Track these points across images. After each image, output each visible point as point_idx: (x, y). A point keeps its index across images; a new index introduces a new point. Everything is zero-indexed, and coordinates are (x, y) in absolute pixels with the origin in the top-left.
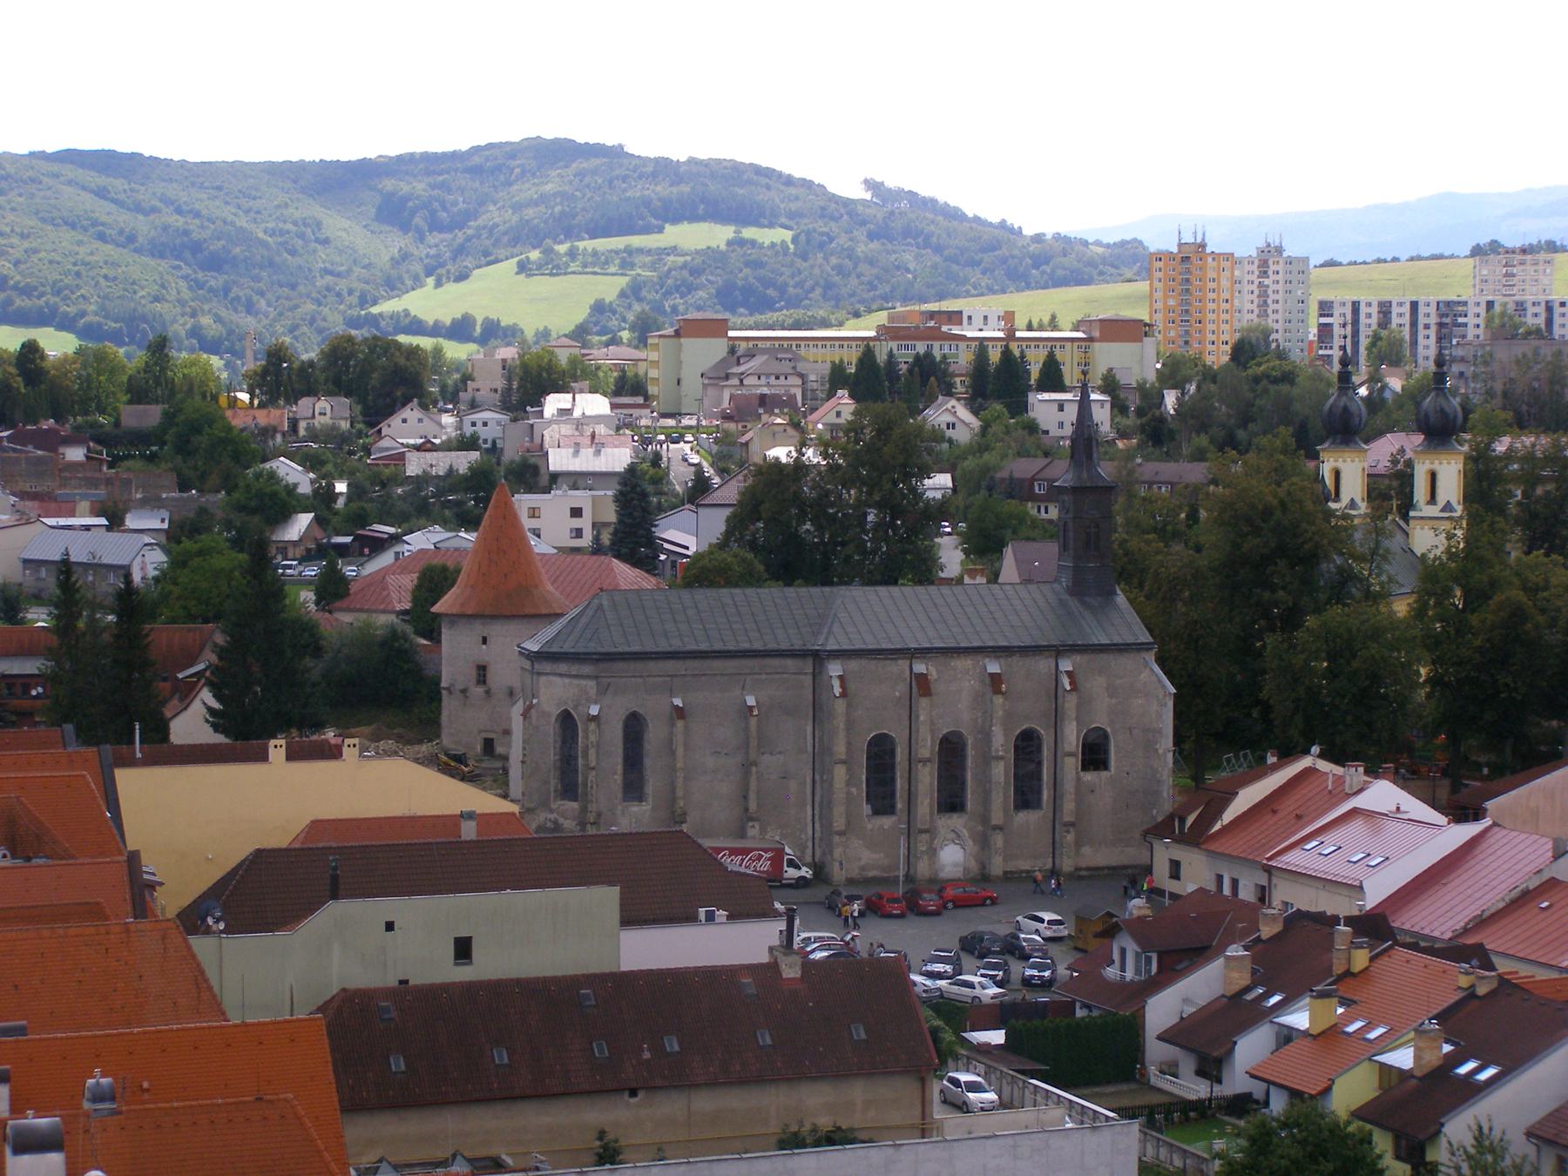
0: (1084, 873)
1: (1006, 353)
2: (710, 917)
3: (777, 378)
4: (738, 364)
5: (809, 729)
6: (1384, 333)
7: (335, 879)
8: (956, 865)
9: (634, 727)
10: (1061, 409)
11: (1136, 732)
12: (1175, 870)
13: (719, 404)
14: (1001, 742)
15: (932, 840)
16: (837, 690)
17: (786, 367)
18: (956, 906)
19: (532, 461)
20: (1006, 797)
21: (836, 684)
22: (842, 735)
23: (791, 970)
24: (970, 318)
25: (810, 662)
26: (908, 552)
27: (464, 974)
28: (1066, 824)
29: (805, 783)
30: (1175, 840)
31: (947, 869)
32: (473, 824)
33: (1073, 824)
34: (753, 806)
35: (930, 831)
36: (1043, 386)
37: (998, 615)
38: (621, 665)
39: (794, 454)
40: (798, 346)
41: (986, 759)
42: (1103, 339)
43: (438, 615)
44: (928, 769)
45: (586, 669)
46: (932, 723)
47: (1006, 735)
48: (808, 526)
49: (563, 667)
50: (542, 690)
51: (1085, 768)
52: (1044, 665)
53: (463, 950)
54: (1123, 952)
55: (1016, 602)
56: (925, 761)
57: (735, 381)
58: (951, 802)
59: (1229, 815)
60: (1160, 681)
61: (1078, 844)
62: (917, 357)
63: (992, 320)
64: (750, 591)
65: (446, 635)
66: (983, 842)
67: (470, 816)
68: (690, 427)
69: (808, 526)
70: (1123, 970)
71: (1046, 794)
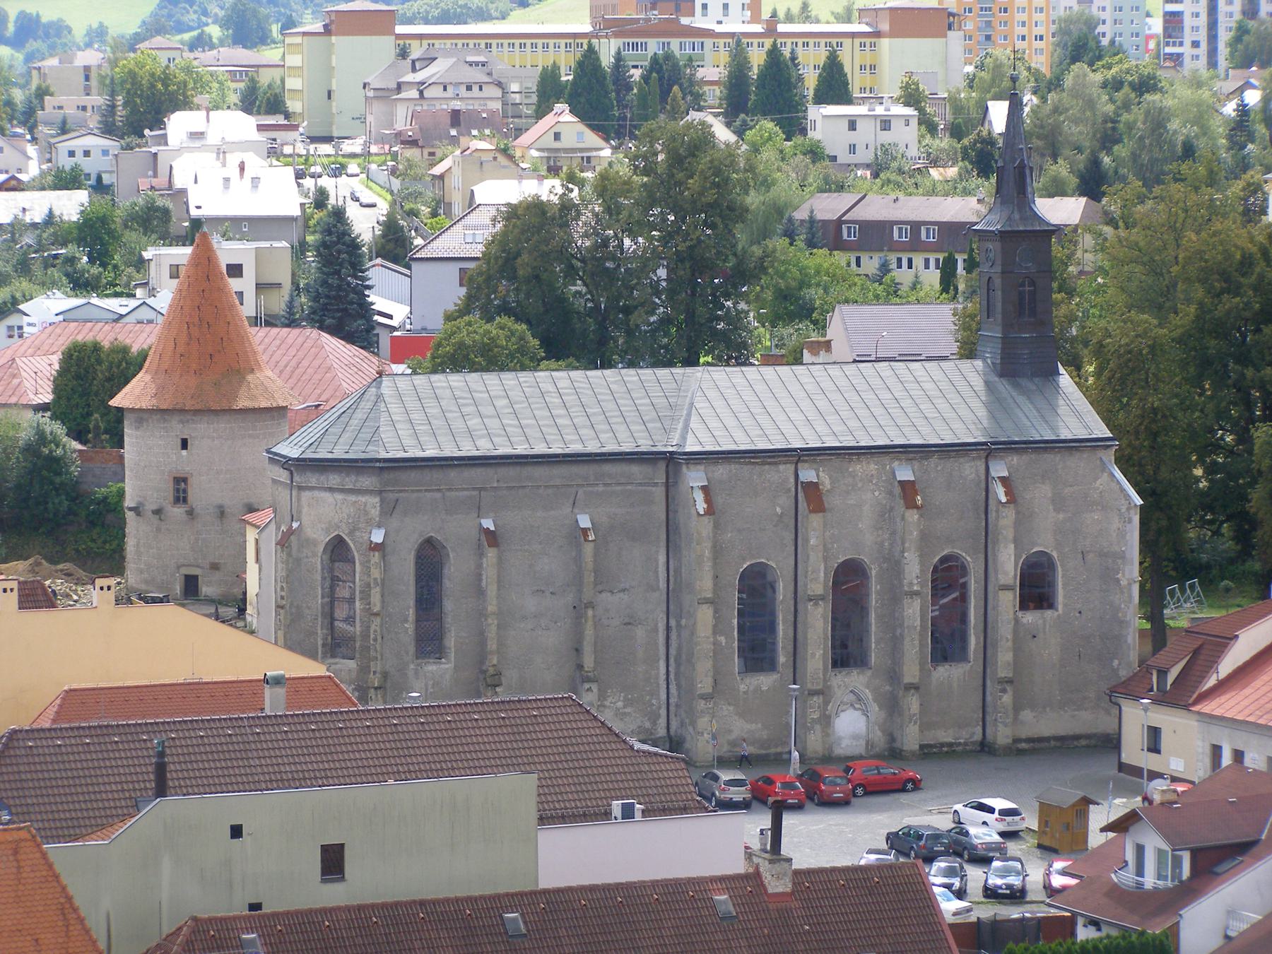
0: (1024, 745)
1: (774, 53)
2: (628, 813)
3: (469, 88)
4: (414, 70)
5: (662, 559)
6: (1252, 24)
7: (161, 770)
8: (855, 737)
9: (430, 562)
10: (852, 126)
12: (1154, 740)
13: (390, 125)
14: (915, 571)
15: (826, 703)
16: (701, 506)
17: (478, 75)
18: (867, 793)
19: (160, 202)
20: (922, 645)
21: (699, 497)
22: (708, 565)
23: (777, 885)
24: (705, 6)
25: (662, 466)
26: (719, 319)
27: (334, 895)
28: (1002, 681)
29: (656, 630)
30: (1157, 701)
32: (281, 691)
33: (1010, 681)
34: (589, 662)
35: (824, 692)
36: (821, 99)
37: (906, 403)
38: (413, 475)
39: (560, 191)
40: (488, 46)
41: (895, 596)
42: (893, 34)
43: (120, 410)
44: (820, 610)
45: (367, 481)
46: (826, 549)
47: (922, 563)
48: (579, 287)
49: (334, 479)
50: (305, 510)
51: (1024, 606)
52: (970, 469)
53: (333, 862)
54: (1140, 850)
55: (928, 386)
56: (815, 599)
57: (414, 94)
58: (846, 654)
59: (1227, 665)
60: (1122, 490)
61: (1017, 708)
62: (655, 59)
63: (735, 9)
64: (525, 377)
65: (130, 434)
66: (892, 706)
67: (278, 681)
68: (353, 156)
69: (579, 287)
70: (1140, 871)
71: (973, 642)
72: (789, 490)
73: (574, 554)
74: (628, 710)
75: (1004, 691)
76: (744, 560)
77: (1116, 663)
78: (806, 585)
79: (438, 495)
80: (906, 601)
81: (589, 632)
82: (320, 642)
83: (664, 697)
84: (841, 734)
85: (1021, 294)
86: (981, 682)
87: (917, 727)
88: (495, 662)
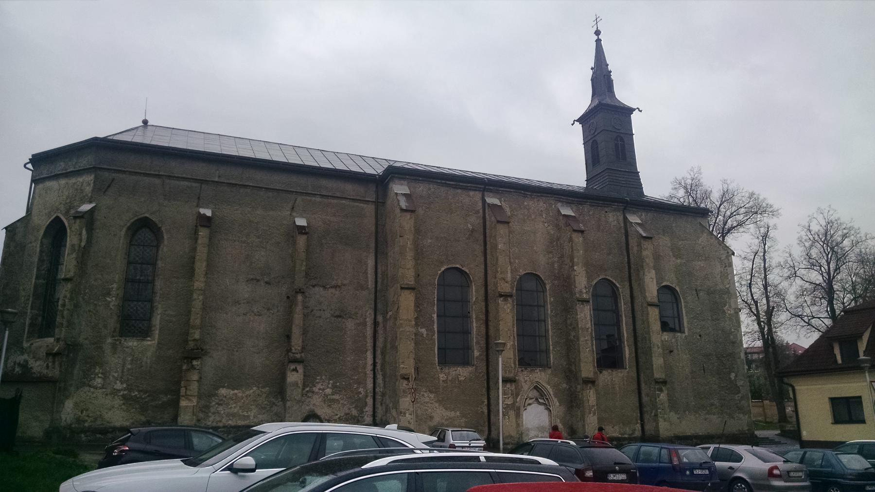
5: (371, 263)
8: (541, 429)
9: (144, 229)
11: (701, 294)
29: (365, 324)
31: (532, 433)
34: (297, 342)
41: (567, 307)
58: (530, 357)
66: (572, 402)
72: (478, 212)
73: (290, 251)
74: (336, 397)
75: (661, 390)
76: (442, 263)
77: (733, 376)
78: (496, 285)
79: (157, 181)
80: (579, 307)
81: (298, 318)
82: (28, 322)
83: (370, 385)
84: (530, 426)
85: (616, 145)
86: (636, 386)
87: (596, 417)
88: (197, 336)
